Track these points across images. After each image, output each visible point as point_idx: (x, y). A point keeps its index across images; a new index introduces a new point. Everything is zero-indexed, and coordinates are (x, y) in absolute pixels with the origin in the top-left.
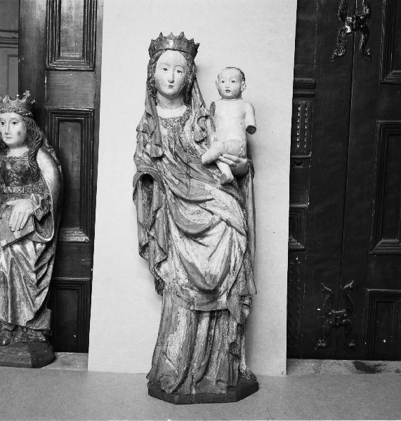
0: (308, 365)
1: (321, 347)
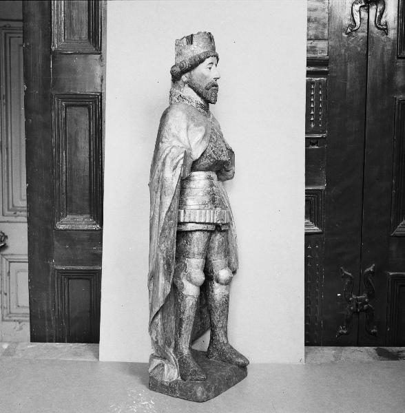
0: (328, 352)
1: (342, 334)
